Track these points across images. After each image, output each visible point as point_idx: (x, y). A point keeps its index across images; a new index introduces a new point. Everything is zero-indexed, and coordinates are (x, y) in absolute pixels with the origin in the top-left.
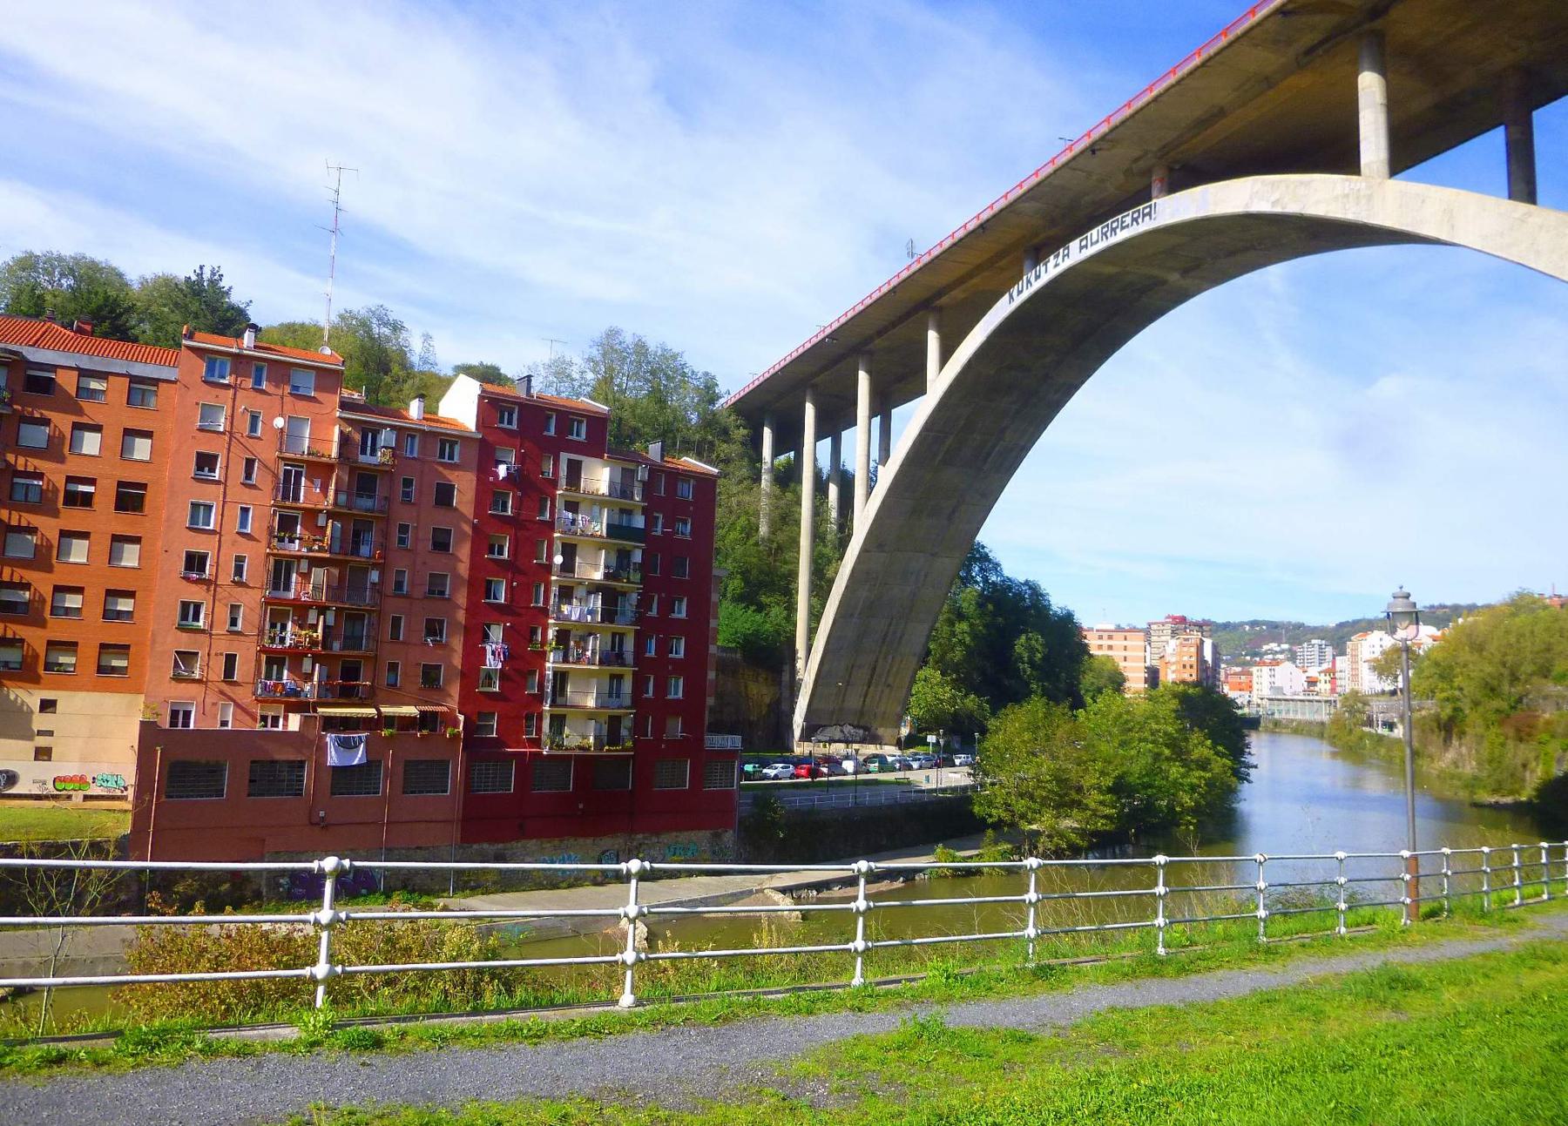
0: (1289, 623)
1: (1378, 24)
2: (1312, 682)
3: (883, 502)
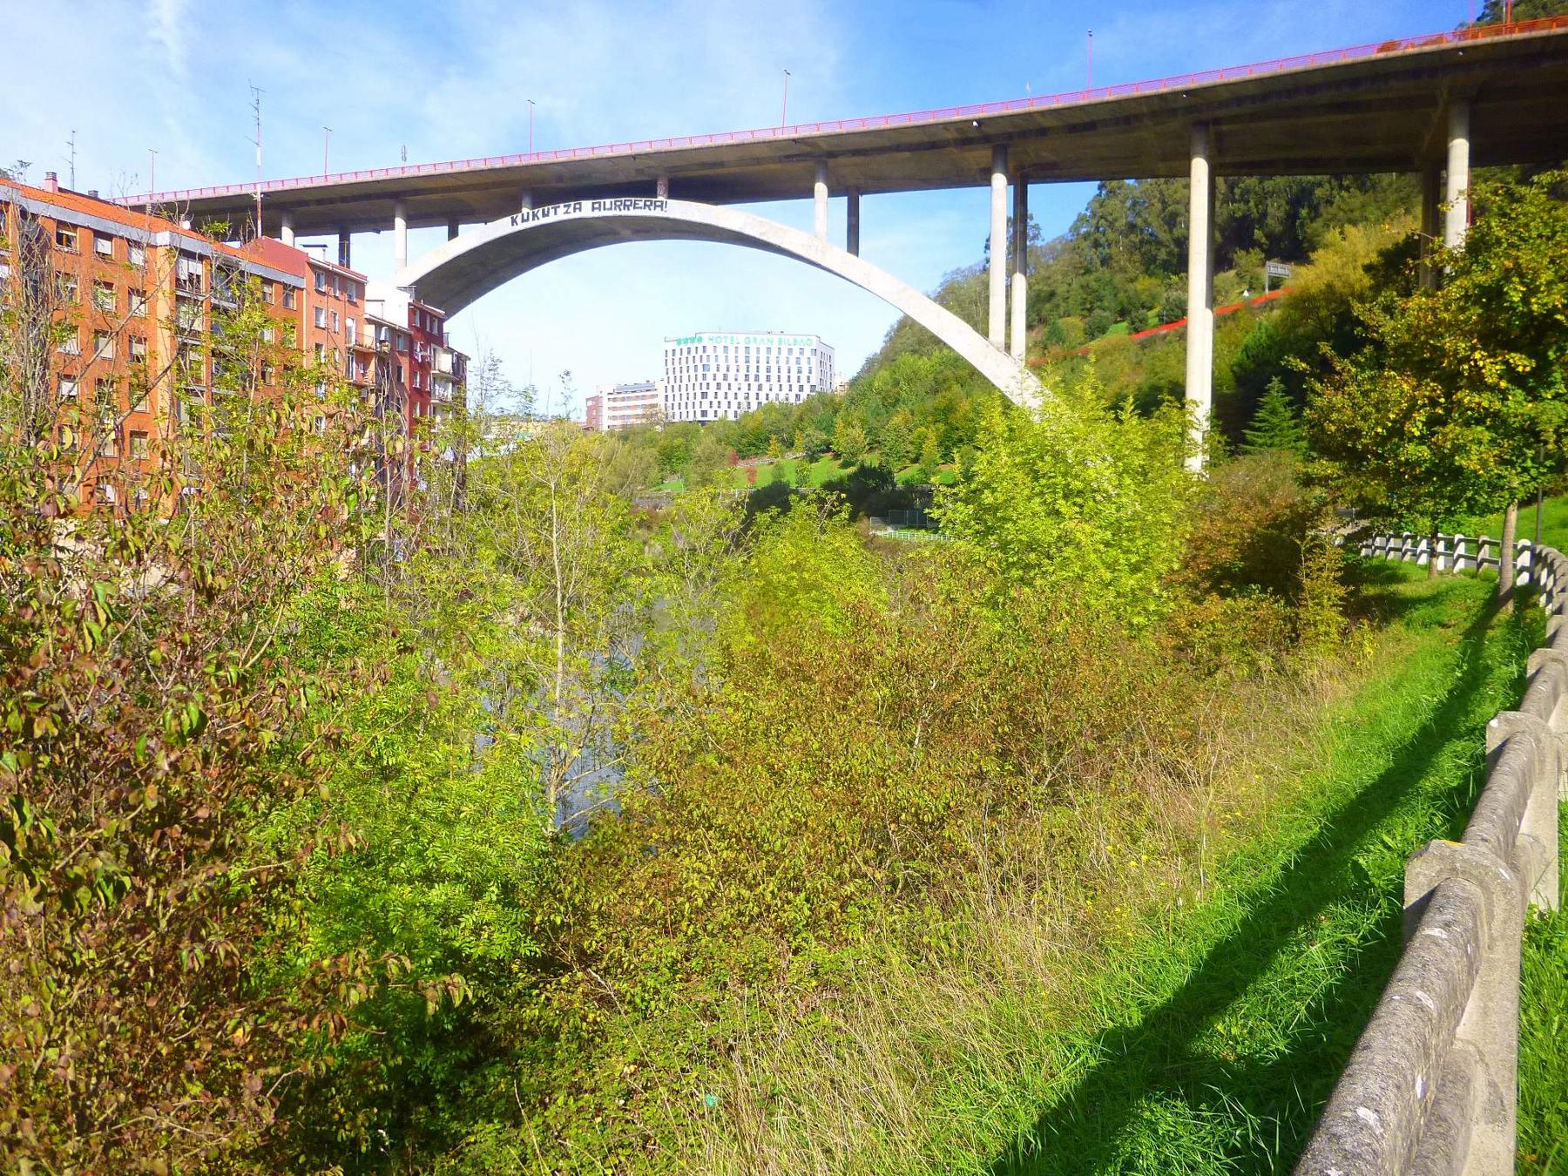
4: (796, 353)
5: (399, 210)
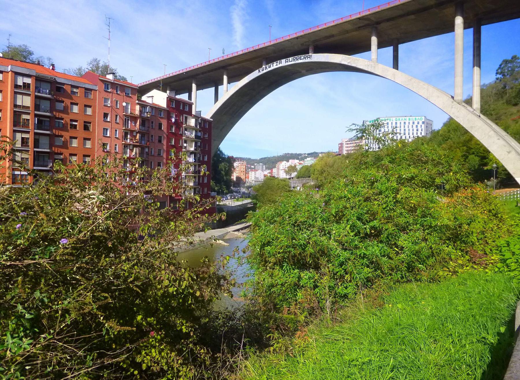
1: (377, 26)
4: (416, 123)
5: (225, 73)
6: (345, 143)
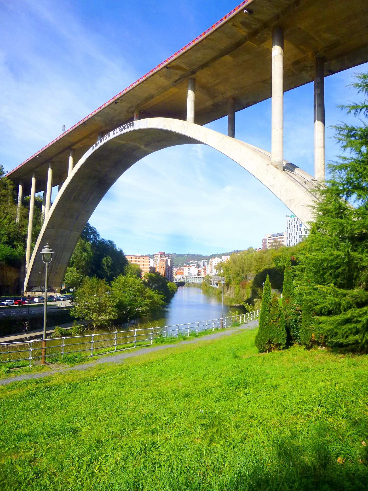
0: (198, 255)
1: (194, 76)
2: (200, 272)
3: (53, 212)
6: (268, 239)
